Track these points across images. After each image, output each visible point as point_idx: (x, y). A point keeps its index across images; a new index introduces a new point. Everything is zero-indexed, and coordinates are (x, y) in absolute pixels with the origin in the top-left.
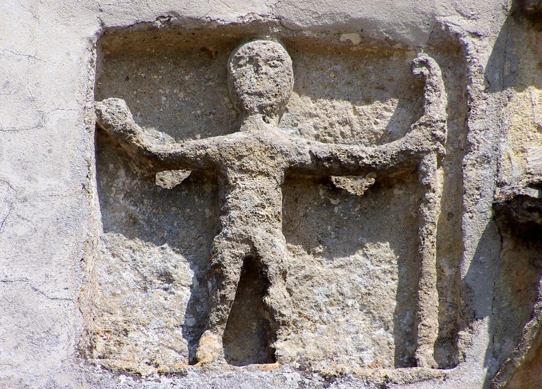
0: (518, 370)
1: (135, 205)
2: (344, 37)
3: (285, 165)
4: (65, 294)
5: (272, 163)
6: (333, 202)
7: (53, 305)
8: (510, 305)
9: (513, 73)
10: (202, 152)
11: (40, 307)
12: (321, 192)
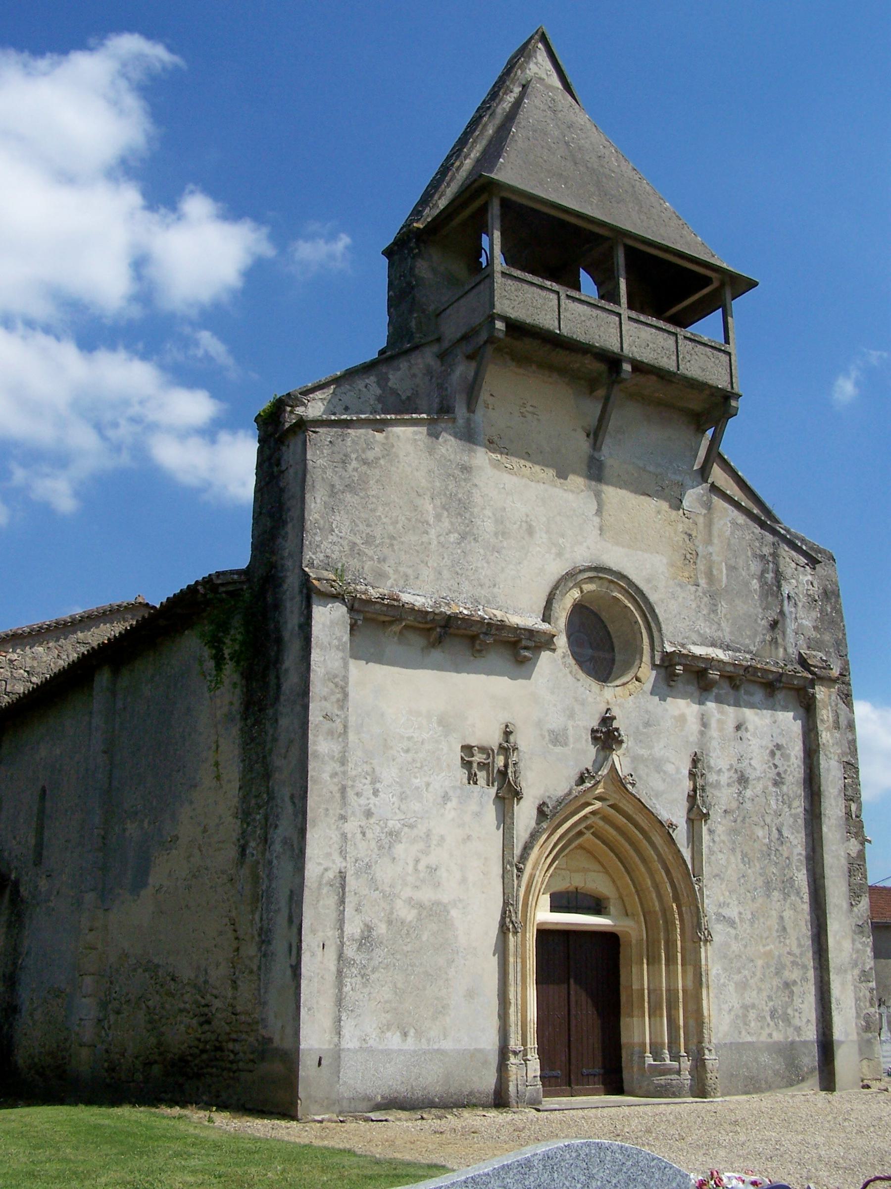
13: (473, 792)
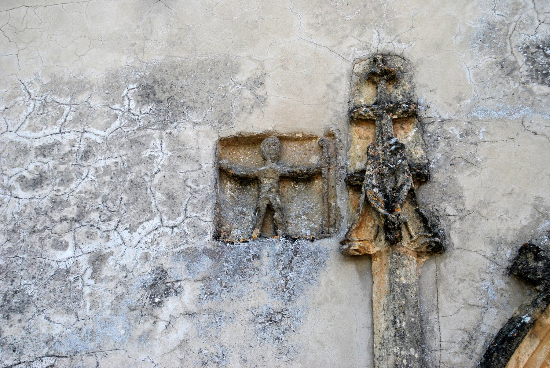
0: (354, 230)
1: (233, 192)
2: (297, 135)
3: (279, 175)
4: (209, 220)
5: (275, 175)
6: (296, 187)
7: (206, 223)
8: (352, 212)
9: (350, 140)
10: (253, 173)
11: (201, 224)
12: (292, 184)
13: (256, 257)
